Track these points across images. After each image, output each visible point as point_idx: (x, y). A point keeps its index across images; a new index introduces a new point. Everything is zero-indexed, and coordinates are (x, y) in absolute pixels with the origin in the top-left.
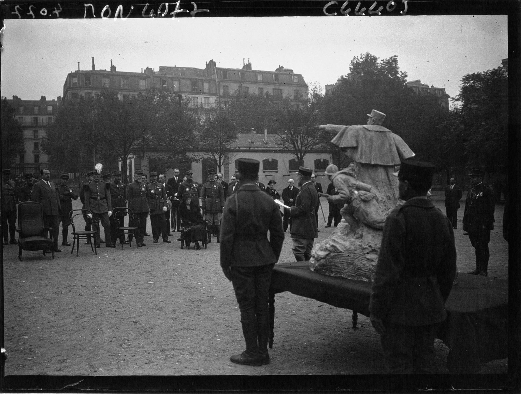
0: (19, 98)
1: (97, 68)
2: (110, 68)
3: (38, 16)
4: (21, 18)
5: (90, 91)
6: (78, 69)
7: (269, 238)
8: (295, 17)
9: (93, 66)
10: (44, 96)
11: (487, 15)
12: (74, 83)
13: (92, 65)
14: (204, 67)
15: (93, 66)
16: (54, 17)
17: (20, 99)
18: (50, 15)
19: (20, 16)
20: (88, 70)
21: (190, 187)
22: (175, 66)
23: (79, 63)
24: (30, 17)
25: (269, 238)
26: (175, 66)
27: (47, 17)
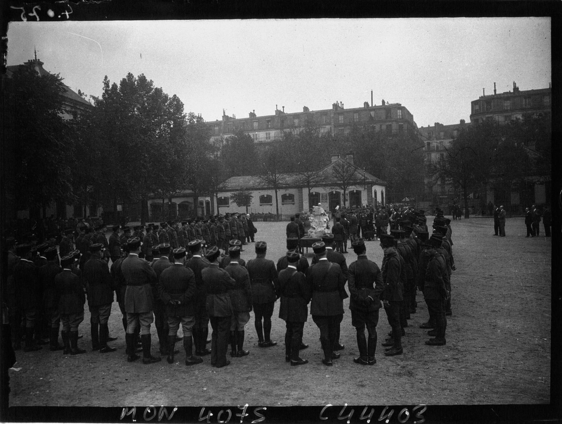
0: (441, 124)
1: (497, 93)
2: (363, 105)
3: (44, 18)
4: (40, 20)
5: (491, 115)
6: (483, 95)
7: (99, 326)
8: (377, 19)
9: (495, 91)
10: (462, 119)
11: (530, 17)
12: (476, 110)
13: (494, 89)
14: (363, 106)
15: (495, 91)
16: (64, 19)
17: (442, 125)
18: (59, 17)
19: (38, 19)
20: (491, 94)
21: (378, 215)
22: (383, 102)
23: (484, 89)
24: (33, 19)
25: (99, 326)
26: (383, 102)
27: (55, 19)
